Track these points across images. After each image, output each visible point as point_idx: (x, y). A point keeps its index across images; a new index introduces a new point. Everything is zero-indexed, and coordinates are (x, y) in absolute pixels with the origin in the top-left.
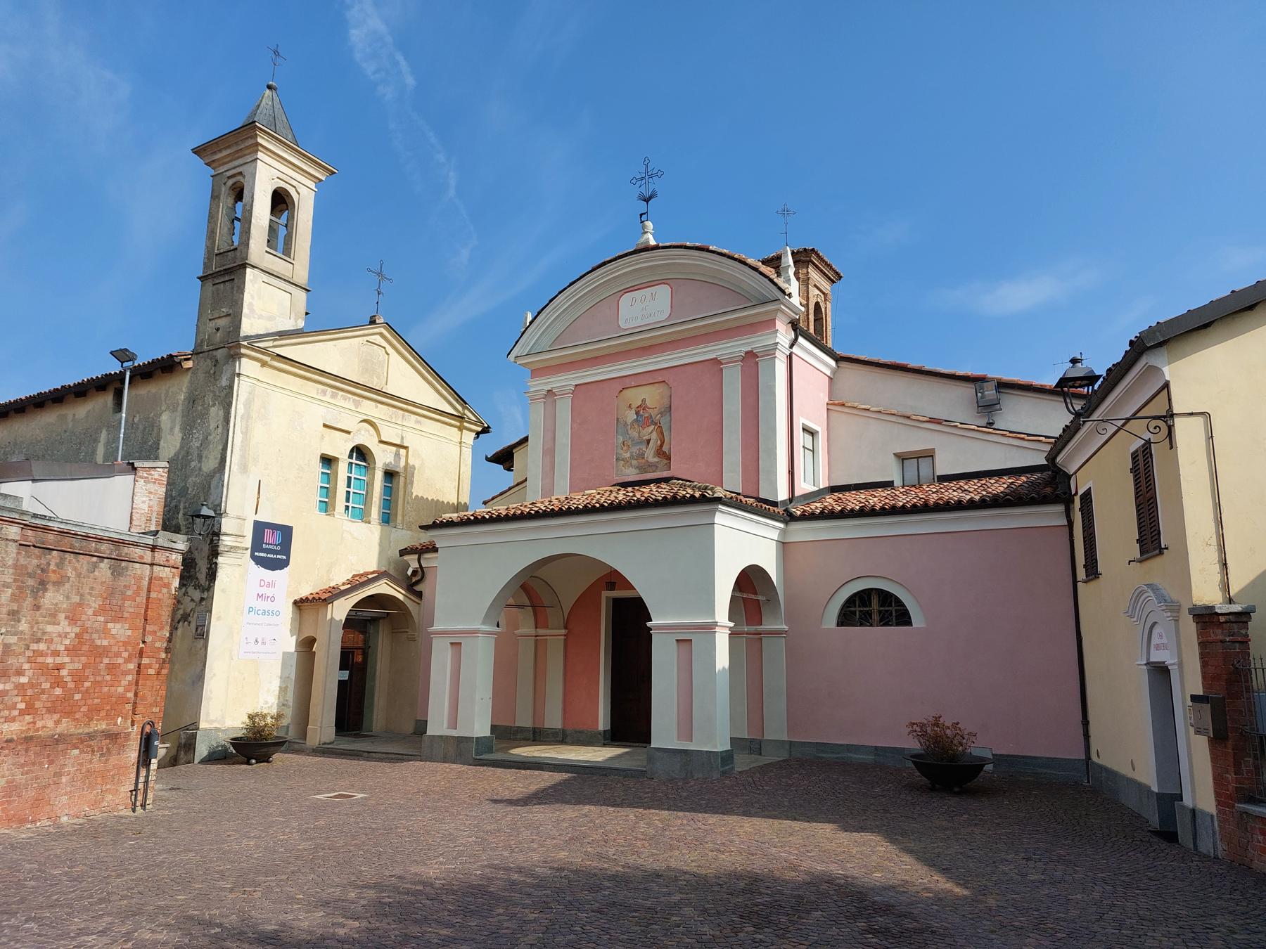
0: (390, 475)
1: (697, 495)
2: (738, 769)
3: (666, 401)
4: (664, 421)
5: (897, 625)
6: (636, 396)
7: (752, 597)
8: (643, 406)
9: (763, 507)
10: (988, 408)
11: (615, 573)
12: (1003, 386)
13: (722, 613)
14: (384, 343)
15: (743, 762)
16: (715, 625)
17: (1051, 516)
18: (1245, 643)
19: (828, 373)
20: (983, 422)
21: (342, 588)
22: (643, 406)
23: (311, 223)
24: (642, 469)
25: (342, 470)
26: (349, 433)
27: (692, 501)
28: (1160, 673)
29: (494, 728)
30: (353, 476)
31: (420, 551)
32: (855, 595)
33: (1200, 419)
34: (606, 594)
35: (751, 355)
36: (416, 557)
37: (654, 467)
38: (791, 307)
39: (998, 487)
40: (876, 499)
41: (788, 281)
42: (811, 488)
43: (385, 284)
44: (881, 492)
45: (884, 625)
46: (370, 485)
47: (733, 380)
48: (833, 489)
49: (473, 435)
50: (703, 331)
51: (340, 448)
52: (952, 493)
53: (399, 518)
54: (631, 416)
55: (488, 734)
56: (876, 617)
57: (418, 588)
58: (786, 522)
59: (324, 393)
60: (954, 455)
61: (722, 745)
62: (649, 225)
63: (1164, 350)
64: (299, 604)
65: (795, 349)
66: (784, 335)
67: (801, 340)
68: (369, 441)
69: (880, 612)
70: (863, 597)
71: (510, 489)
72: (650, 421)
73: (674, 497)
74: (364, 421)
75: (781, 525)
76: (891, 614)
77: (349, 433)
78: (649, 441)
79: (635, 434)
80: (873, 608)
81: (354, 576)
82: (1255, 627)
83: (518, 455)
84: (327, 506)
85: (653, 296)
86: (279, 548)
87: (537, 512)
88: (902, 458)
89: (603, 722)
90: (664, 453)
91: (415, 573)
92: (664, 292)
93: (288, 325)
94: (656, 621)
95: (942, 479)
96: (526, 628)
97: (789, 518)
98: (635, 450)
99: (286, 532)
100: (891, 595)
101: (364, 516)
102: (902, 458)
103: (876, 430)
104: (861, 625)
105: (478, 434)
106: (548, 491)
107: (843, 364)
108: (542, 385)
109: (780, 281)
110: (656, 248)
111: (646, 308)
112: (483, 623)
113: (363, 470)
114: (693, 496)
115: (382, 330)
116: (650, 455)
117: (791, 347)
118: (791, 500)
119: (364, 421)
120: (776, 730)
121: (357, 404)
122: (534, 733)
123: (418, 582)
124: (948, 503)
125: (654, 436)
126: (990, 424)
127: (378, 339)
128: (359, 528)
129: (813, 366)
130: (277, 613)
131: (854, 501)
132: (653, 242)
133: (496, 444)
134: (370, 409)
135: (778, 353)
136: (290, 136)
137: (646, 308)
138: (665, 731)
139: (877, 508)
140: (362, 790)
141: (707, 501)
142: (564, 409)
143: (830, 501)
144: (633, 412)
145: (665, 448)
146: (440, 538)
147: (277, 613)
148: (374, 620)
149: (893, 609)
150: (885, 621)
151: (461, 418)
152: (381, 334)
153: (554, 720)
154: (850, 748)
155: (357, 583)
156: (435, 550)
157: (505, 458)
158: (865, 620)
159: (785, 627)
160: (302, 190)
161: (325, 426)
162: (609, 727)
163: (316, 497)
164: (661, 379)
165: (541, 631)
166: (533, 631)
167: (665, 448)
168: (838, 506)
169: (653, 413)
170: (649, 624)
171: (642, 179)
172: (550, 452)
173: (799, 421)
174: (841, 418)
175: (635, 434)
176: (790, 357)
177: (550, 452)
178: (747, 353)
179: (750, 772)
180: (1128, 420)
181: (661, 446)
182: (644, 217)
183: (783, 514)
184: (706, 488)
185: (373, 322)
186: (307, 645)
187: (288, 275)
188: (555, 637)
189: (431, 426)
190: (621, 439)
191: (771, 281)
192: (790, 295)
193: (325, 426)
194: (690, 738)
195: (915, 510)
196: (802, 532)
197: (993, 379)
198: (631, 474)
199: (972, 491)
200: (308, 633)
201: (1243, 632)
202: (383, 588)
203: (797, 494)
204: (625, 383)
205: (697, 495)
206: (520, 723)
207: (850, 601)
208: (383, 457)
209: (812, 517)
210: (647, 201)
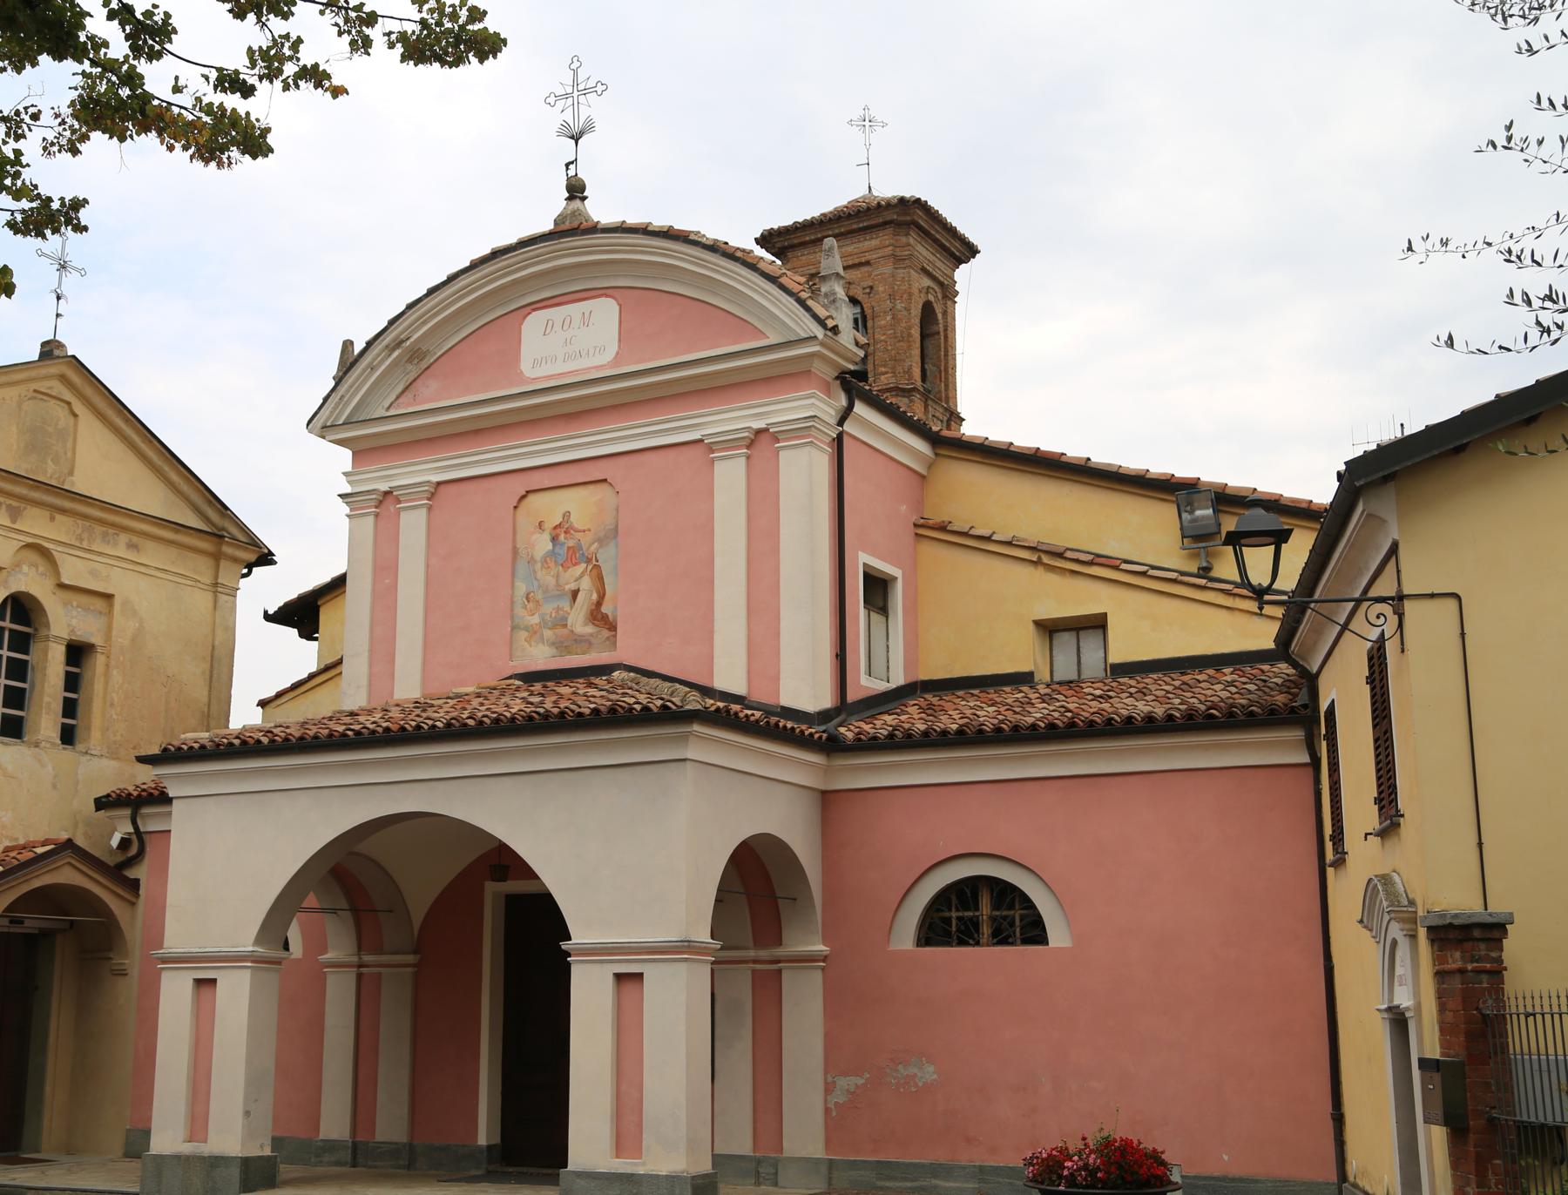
0: (77, 653)
4: (607, 558)
8: (561, 530)
11: (503, 850)
14: (68, 396)
18: (1497, 973)
24: (562, 647)
28: (1399, 1021)
29: (277, 1142)
33: (1453, 603)
36: (128, 812)
37: (583, 643)
42: (881, 686)
43: (71, 279)
44: (1010, 696)
47: (730, 475)
53: (96, 734)
54: (543, 544)
55: (267, 1152)
56: (986, 930)
57: (131, 873)
60: (1147, 628)
63: (1391, 488)
65: (847, 427)
67: (860, 408)
70: (964, 893)
76: (1012, 924)
78: (575, 594)
79: (550, 581)
82: (1513, 947)
83: (327, 616)
85: (586, 321)
89: (485, 1133)
90: (605, 617)
91: (125, 844)
92: (605, 312)
94: (580, 934)
97: (832, 746)
98: (548, 609)
100: (1014, 889)
102: (1050, 629)
104: (962, 943)
116: (578, 621)
117: (841, 423)
119: (28, 546)
121: (14, 514)
124: (1129, 720)
125: (586, 584)
134: (37, 524)
138: (589, 1141)
142: (413, 525)
144: (546, 536)
145: (605, 609)
146: (175, 778)
148: (46, 935)
149: (1017, 914)
150: (1002, 937)
154: (936, 1170)
158: (967, 935)
159: (821, 947)
162: (497, 1140)
165: (367, 958)
167: (605, 609)
169: (585, 540)
170: (565, 945)
171: (566, 96)
173: (861, 559)
174: (935, 555)
175: (550, 581)
180: (1359, 602)
181: (599, 604)
189: (153, 555)
194: (637, 1152)
198: (541, 657)
201: (1494, 954)
202: (67, 875)
207: (942, 899)
210: (576, 138)
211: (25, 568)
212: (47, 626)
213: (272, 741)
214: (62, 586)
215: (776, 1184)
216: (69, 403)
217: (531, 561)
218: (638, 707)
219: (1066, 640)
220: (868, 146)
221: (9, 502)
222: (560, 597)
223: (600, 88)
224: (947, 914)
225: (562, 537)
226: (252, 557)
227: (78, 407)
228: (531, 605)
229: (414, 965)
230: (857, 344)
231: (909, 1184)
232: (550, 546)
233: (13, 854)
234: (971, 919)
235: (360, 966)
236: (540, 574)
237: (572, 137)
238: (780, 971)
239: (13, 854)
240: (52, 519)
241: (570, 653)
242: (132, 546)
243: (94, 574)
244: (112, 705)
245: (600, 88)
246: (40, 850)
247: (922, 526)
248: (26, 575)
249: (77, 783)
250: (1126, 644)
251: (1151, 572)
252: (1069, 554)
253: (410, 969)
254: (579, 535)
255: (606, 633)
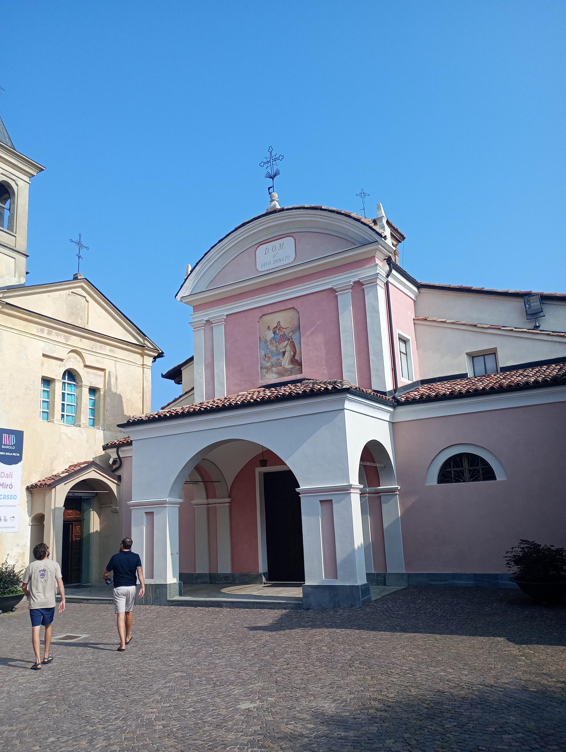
1: (330, 387)
2: (373, 599)
3: (296, 323)
4: (295, 338)
5: (485, 479)
6: (273, 320)
7: (373, 465)
8: (278, 327)
9: (378, 397)
10: (534, 315)
12: (545, 298)
13: (354, 479)
14: (84, 294)
15: (375, 593)
16: (350, 486)
17: (494, 355)
19: (413, 297)
20: (532, 326)
21: (62, 475)
22: (278, 327)
23: (27, 206)
25: (58, 387)
26: (61, 360)
27: (326, 392)
30: (66, 392)
31: (117, 446)
32: (450, 459)
34: (260, 470)
35: (359, 284)
36: (115, 450)
38: (386, 246)
39: (554, 371)
40: (459, 386)
41: (383, 228)
42: (407, 382)
43: (83, 251)
45: (473, 481)
46: (79, 399)
48: (423, 382)
49: (152, 359)
50: (268, 284)
51: (56, 371)
52: (517, 378)
54: (270, 335)
56: (467, 475)
58: (394, 407)
59: (42, 331)
60: (514, 352)
61: (361, 580)
62: (275, 195)
64: (31, 489)
65: (390, 279)
66: (382, 268)
67: (394, 272)
68: (75, 364)
69: (470, 471)
70: (455, 460)
71: (180, 397)
72: (283, 338)
73: (312, 390)
74: (72, 351)
75: (391, 410)
76: (479, 472)
77: (61, 360)
78: (284, 353)
79: (274, 349)
80: (463, 468)
81: (70, 466)
83: (185, 373)
84: (48, 415)
85: (281, 246)
86: (14, 448)
87: (205, 409)
88: (472, 356)
89: (262, 567)
91: (115, 462)
92: (289, 242)
93: (14, 282)
94: (303, 486)
95: (504, 369)
96: (200, 499)
97: (397, 404)
98: (274, 360)
99: (19, 435)
101: (76, 422)
102: (472, 356)
103: (452, 335)
104: (457, 481)
105: (155, 358)
106: (211, 393)
107: (423, 290)
108: (203, 316)
109: (377, 228)
110: (282, 210)
111: (278, 255)
112: (170, 496)
113: (73, 388)
114: (326, 389)
115: (83, 284)
116: (286, 362)
117: (388, 276)
118: (396, 390)
119: (72, 351)
120: (396, 566)
122: (210, 578)
123: (117, 469)
124: (518, 384)
125: (288, 348)
126: (536, 327)
127: (80, 291)
128: (72, 430)
129: (403, 293)
130: (14, 497)
131: (443, 388)
132: (278, 207)
133: (168, 364)
134: (75, 342)
135: (378, 282)
136: (9, 145)
137: (278, 255)
138: (315, 573)
139: (464, 391)
140: (84, 631)
141: (337, 391)
142: (219, 333)
143: (423, 390)
144: (271, 332)
145: (297, 357)
146: (133, 433)
147: (14, 497)
149: (480, 468)
150: (474, 477)
151: (142, 346)
152: (82, 287)
153: (225, 567)
154: (454, 576)
155: (72, 472)
156: (130, 443)
157: (175, 375)
158: (459, 478)
160: (20, 183)
161: (44, 355)
163: (39, 408)
164: (291, 306)
165: (211, 501)
166: (205, 501)
167: (297, 357)
168: (430, 393)
169: (286, 331)
171: (268, 162)
172: (210, 366)
173: (397, 332)
175: (274, 349)
176: (387, 284)
177: (210, 366)
178: (355, 283)
179: (384, 599)
181: (294, 356)
182: (271, 190)
183: (394, 400)
184: (335, 382)
185: (75, 278)
186: (39, 521)
187: (12, 245)
188: (222, 504)
190: (263, 353)
191: (371, 228)
192: (385, 237)
193: (44, 355)
195: (492, 391)
196: (406, 414)
197: (536, 294)
198: (272, 379)
199: (531, 376)
200: (38, 511)
202: (92, 474)
203: (399, 385)
204: (264, 311)
205: (330, 387)
206: (198, 571)
207: (447, 464)
208: (89, 379)
209: (414, 402)
210: (272, 178)
211: (72, 359)
212: (82, 382)
213: (171, 415)
214: (86, 366)
215: (385, 585)
216: (85, 297)
217: (266, 342)
218: (323, 389)
219: (479, 361)
220: (364, 203)
221: (64, 334)
222: (278, 354)
223: (281, 158)
224: (449, 470)
225: (277, 331)
226: (156, 355)
227: (88, 298)
228: (266, 359)
229: (229, 503)
230: (393, 244)
231: (443, 583)
232: (273, 335)
233: (73, 468)
234: (460, 471)
235: (208, 504)
236: (269, 347)
237: (271, 178)
238: (380, 497)
239: (73, 468)
240: (81, 341)
241: (284, 376)
242: (111, 351)
243: (98, 361)
244: (107, 410)
245: (281, 158)
246: (82, 466)
247: (417, 319)
248: (72, 362)
249: (96, 440)
250: (506, 359)
251: (514, 330)
252: (479, 325)
253: (228, 504)
254: (284, 330)
255: (298, 367)
